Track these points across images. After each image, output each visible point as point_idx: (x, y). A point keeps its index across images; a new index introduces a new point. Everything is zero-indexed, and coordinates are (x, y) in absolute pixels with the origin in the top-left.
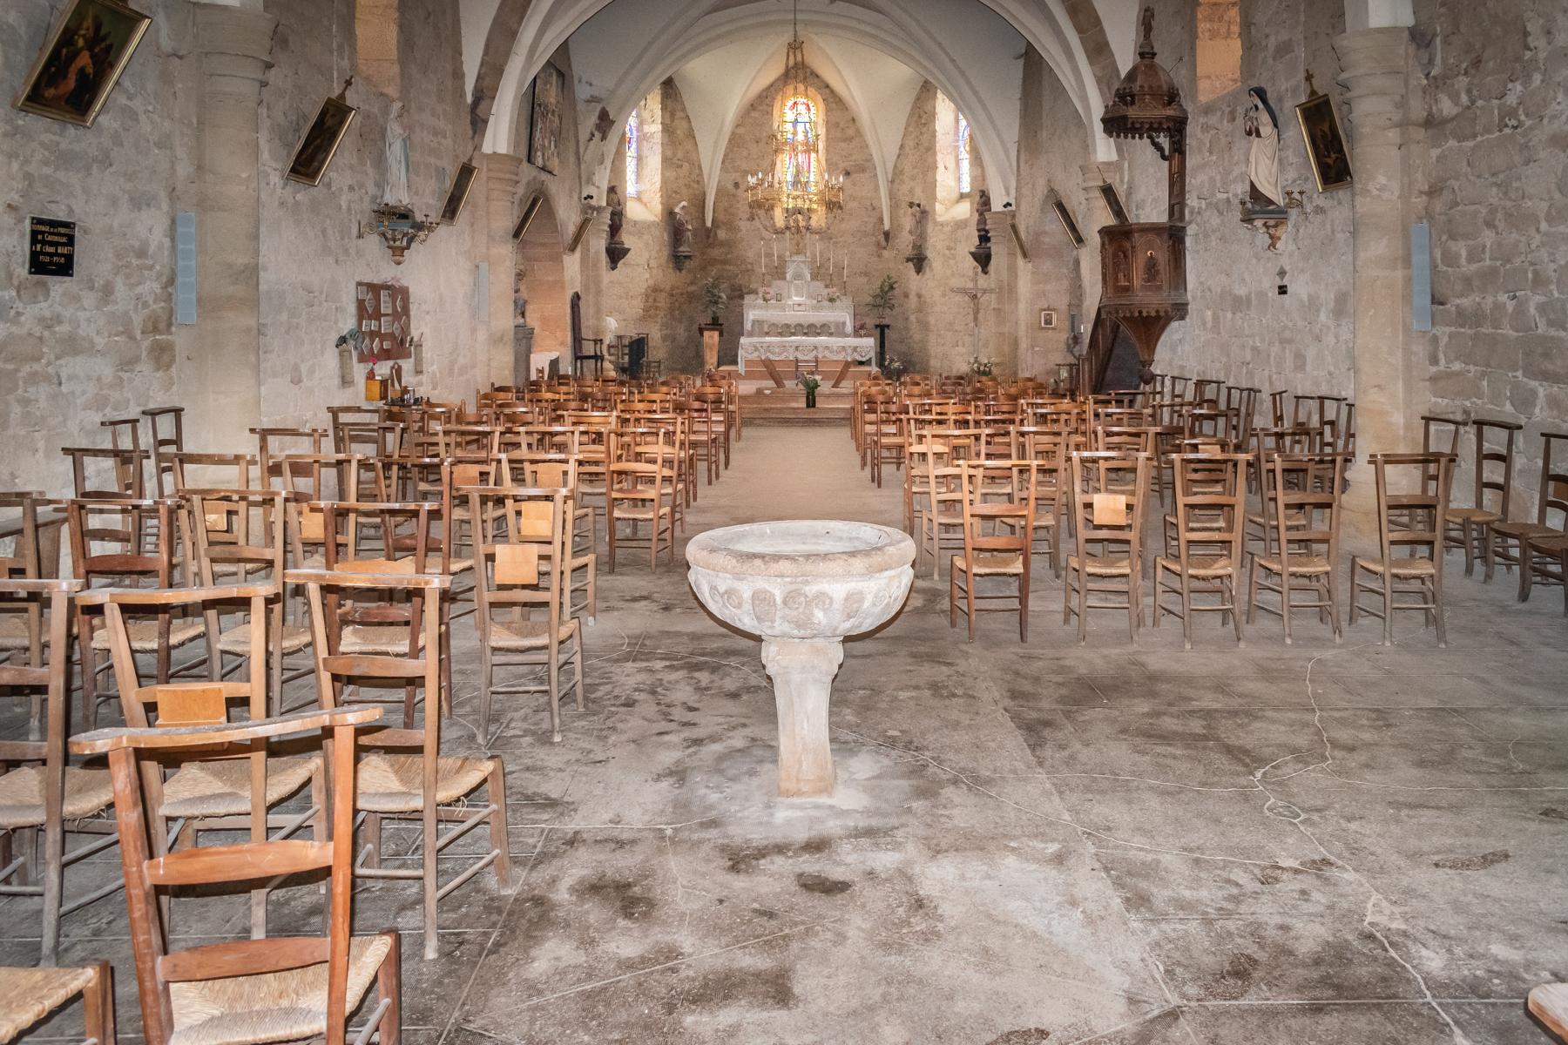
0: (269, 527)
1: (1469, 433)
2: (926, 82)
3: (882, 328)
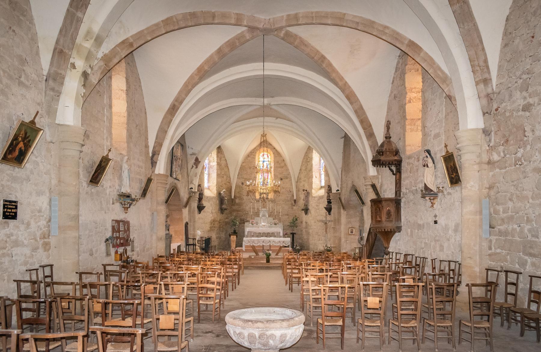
0: (82, 306)
1: (503, 275)
2: (309, 147)
3: (293, 234)
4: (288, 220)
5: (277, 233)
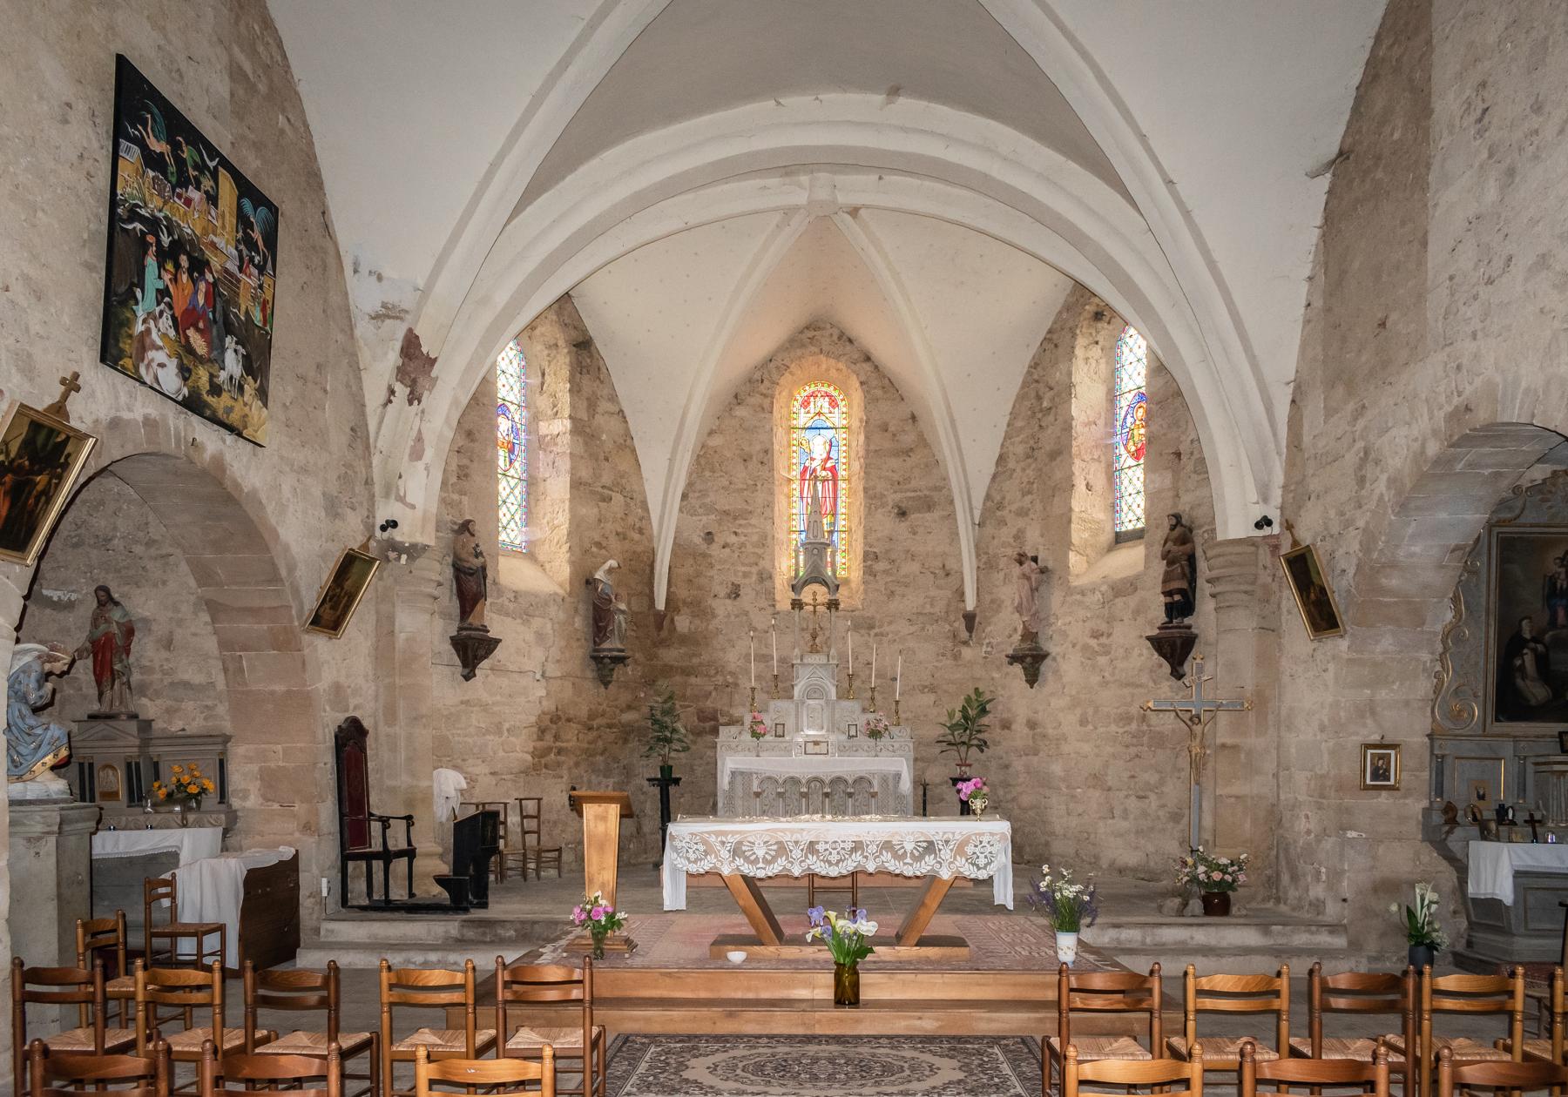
4: (937, 713)
5: (884, 779)
